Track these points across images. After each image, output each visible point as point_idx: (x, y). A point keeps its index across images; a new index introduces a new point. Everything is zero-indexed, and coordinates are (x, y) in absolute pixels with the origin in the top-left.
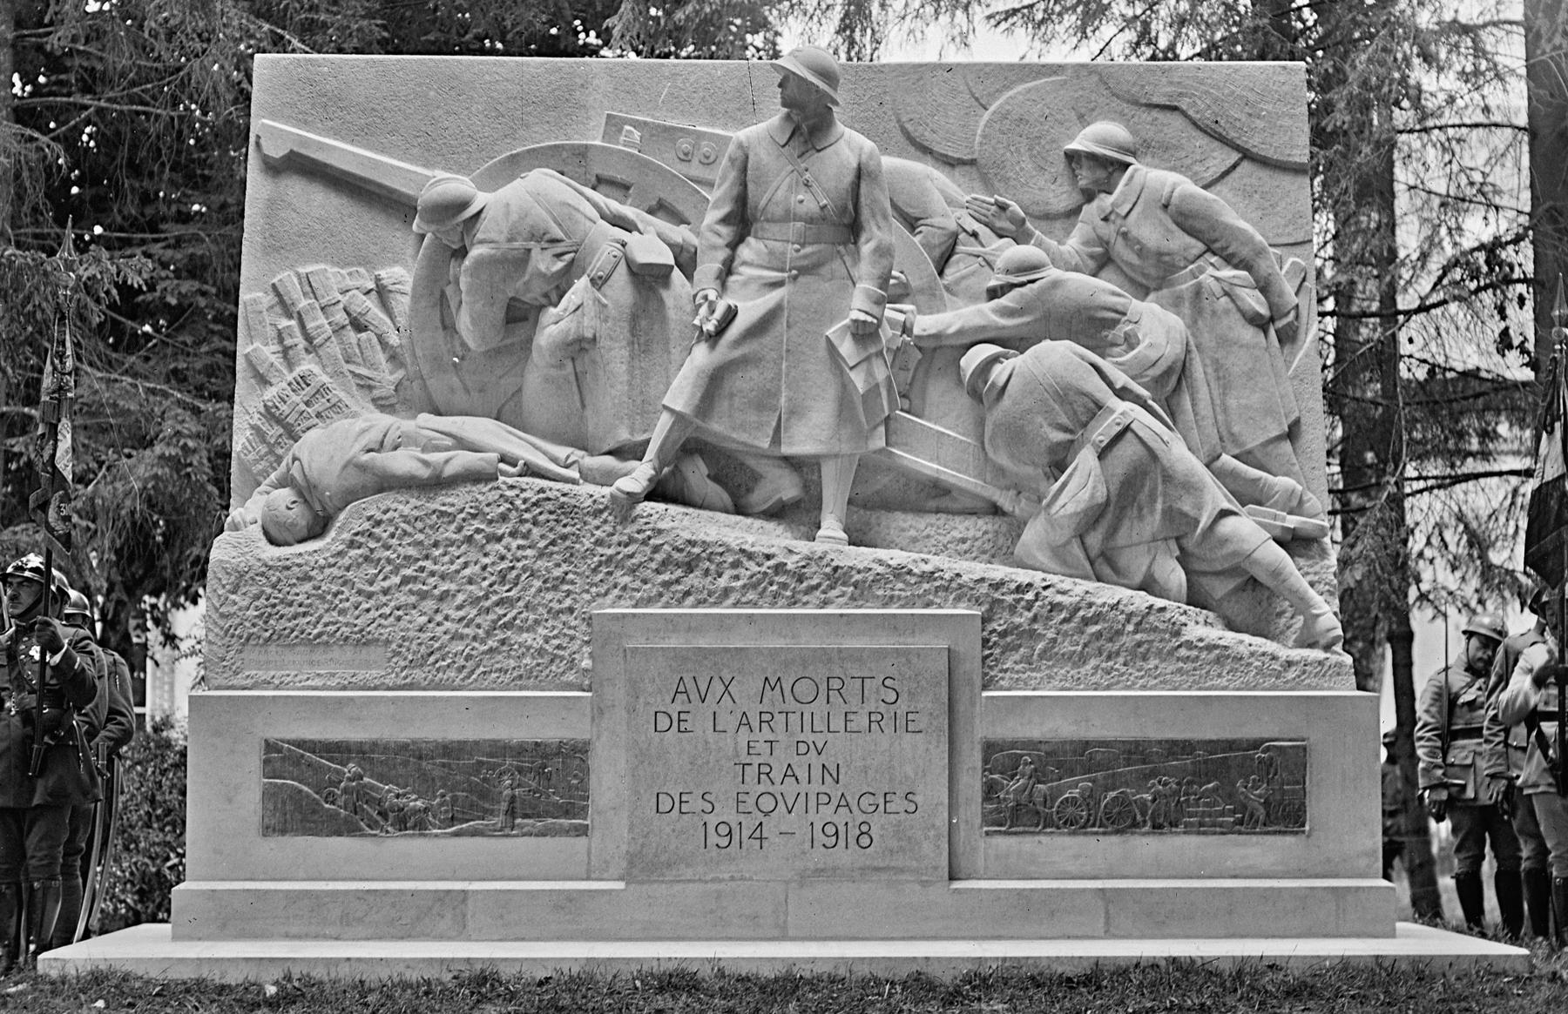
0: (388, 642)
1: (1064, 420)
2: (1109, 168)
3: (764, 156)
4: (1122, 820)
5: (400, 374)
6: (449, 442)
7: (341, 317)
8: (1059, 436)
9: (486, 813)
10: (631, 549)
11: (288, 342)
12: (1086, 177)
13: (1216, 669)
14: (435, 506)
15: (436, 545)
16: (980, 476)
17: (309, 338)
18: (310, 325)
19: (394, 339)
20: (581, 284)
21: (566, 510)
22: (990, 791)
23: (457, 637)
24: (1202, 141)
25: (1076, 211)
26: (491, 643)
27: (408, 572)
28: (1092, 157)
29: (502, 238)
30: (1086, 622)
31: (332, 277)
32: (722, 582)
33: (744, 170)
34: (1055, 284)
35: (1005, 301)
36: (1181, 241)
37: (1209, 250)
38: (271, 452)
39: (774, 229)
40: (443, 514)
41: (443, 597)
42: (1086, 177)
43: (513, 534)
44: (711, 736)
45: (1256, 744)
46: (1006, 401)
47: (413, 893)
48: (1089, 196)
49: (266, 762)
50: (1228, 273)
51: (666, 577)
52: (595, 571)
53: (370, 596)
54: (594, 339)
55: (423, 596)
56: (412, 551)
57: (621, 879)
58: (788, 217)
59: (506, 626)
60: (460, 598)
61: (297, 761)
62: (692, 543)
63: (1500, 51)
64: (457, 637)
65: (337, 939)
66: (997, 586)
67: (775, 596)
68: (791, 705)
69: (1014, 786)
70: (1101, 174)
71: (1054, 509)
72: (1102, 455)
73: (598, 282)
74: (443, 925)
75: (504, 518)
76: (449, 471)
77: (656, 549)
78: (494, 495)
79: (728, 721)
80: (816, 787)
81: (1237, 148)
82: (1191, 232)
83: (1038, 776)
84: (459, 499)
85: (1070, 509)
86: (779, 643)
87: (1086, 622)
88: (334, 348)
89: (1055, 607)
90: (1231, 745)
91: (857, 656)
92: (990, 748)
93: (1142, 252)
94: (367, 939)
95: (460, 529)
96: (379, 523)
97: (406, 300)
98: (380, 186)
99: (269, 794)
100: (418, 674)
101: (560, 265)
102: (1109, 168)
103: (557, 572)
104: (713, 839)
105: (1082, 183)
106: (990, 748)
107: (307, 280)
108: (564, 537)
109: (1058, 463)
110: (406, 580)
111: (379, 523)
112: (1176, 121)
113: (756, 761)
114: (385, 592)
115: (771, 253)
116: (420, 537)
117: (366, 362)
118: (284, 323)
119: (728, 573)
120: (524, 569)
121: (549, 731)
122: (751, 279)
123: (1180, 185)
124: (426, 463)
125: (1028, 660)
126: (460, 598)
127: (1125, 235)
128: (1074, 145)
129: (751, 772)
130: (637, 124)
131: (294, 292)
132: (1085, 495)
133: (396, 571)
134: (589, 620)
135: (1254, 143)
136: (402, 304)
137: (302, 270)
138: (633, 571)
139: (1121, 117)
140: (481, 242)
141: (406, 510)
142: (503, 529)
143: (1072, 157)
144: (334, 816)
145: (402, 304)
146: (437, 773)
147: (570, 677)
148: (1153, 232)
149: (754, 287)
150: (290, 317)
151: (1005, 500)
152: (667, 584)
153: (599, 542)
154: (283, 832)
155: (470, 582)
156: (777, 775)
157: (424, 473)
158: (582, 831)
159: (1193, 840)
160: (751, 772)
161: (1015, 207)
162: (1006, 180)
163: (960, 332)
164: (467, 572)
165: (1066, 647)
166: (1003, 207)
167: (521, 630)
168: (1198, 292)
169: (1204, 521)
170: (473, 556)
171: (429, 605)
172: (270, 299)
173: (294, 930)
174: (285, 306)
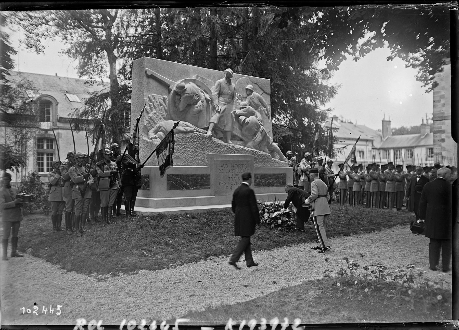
0: (181, 158)
1: (257, 128)
2: (251, 91)
3: (224, 84)
4: (268, 185)
5: (166, 114)
6: (186, 126)
7: (159, 103)
8: (256, 130)
9: (197, 186)
10: (211, 144)
11: (152, 107)
12: (248, 93)
13: (275, 164)
14: (186, 136)
15: (187, 142)
16: (241, 135)
17: (154, 106)
18: (155, 104)
19: (166, 108)
20: (200, 102)
21: (203, 138)
22: (255, 181)
23: (190, 157)
24: (259, 89)
25: (246, 97)
26: (195, 159)
27: (183, 147)
28: (250, 90)
29: (190, 93)
30: (263, 157)
31: (157, 96)
32: (223, 150)
33: (220, 87)
34: (249, 108)
35: (244, 109)
36: (259, 103)
37: (262, 105)
38: (151, 125)
39: (226, 96)
40: (188, 137)
41: (189, 151)
42: (248, 93)
43: (197, 141)
44: (226, 173)
45: (281, 174)
46: (249, 125)
47: (189, 199)
48: (248, 95)
49: (168, 178)
50: (264, 108)
51: (216, 149)
52: (207, 147)
53: (178, 150)
54: (390, 121)
55: (185, 151)
56: (184, 143)
57: (214, 195)
58: (228, 94)
59: (197, 156)
60: (190, 151)
61: (172, 178)
62: (219, 144)
63: (77, 60)
64: (190, 157)
65: (179, 207)
66: (253, 151)
67: (229, 152)
68: (235, 169)
69: (258, 180)
70: (250, 92)
71: (255, 140)
72: (261, 133)
73: (202, 102)
74: (193, 204)
75: (195, 138)
76: (188, 130)
77: (215, 144)
78: (194, 135)
79: (227, 171)
80: (237, 181)
81: (263, 91)
82: (260, 102)
83: (260, 179)
84: (189, 135)
85: (258, 141)
86: (232, 159)
87: (263, 157)
88: (158, 108)
89: (259, 155)
90: (279, 174)
91: (242, 161)
92: (255, 175)
93: (255, 104)
94: (183, 207)
95: (190, 140)
96: (179, 138)
97: (168, 101)
98: (164, 82)
99: (168, 183)
100: (185, 164)
101: (197, 98)
102: (251, 91)
103: (203, 147)
104: (226, 189)
105: (248, 93)
106: (255, 175)
107: (154, 97)
108: (203, 142)
109: (255, 135)
110: (183, 148)
111: (179, 138)
112: (257, 85)
113: (231, 177)
114: (181, 150)
115: (225, 100)
116: (185, 141)
117: (162, 111)
118: (150, 104)
119: (223, 148)
120: (199, 147)
121: (204, 172)
122: (222, 104)
123: (258, 95)
124: (185, 129)
125: (256, 162)
126: (190, 151)
127: (253, 101)
128: (247, 87)
129: (230, 179)
130: (200, 77)
131: (152, 98)
132: (260, 139)
133: (182, 146)
134: (207, 155)
135: (265, 90)
136: (167, 102)
137: (153, 95)
138: (212, 148)
139: (251, 84)
140: (187, 93)
141: (183, 136)
142: (196, 140)
143: (247, 89)
144: (177, 187)
145: (167, 102)
146: (191, 179)
147: (205, 164)
148: (256, 101)
149: (223, 105)
150: (151, 103)
151: (244, 139)
152: (216, 150)
153: (208, 143)
154: (170, 190)
155: (192, 148)
156: (233, 179)
157: (185, 131)
158: (209, 188)
159: (275, 187)
160: (230, 179)
161: (241, 96)
162: (239, 92)
163: (239, 114)
164: (191, 147)
165: (260, 161)
166: (240, 96)
167: (198, 156)
168: (261, 110)
169: (271, 143)
170: (192, 144)
171: (186, 152)
172: (148, 99)
173: (173, 206)
174: (150, 101)
